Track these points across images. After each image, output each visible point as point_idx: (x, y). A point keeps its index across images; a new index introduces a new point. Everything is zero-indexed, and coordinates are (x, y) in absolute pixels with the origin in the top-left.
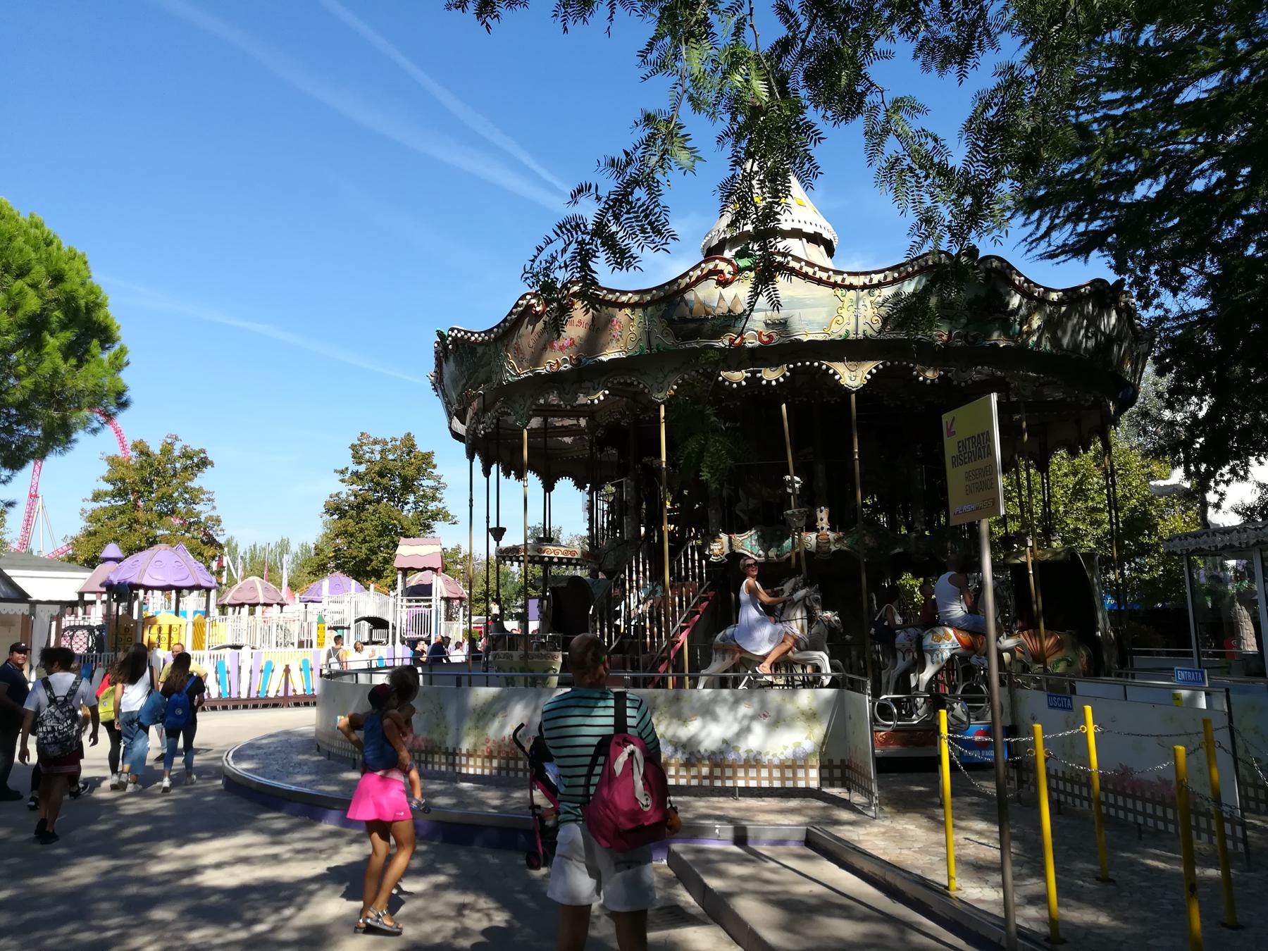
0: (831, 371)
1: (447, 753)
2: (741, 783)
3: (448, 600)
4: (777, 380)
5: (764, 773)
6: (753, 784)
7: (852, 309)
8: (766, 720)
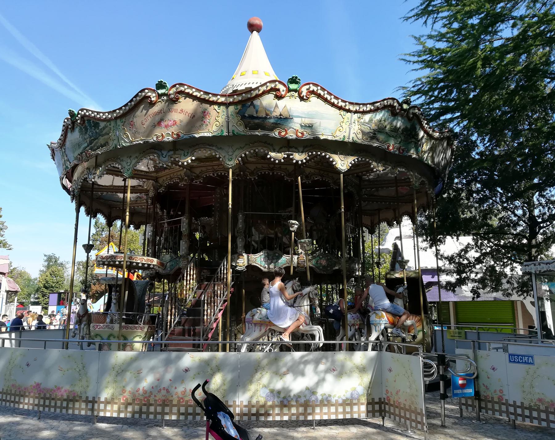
0: (331, 159)
1: (87, 401)
2: (318, 417)
3: (8, 292)
4: (305, 159)
5: (333, 409)
6: (325, 417)
7: (348, 124)
8: (335, 373)
